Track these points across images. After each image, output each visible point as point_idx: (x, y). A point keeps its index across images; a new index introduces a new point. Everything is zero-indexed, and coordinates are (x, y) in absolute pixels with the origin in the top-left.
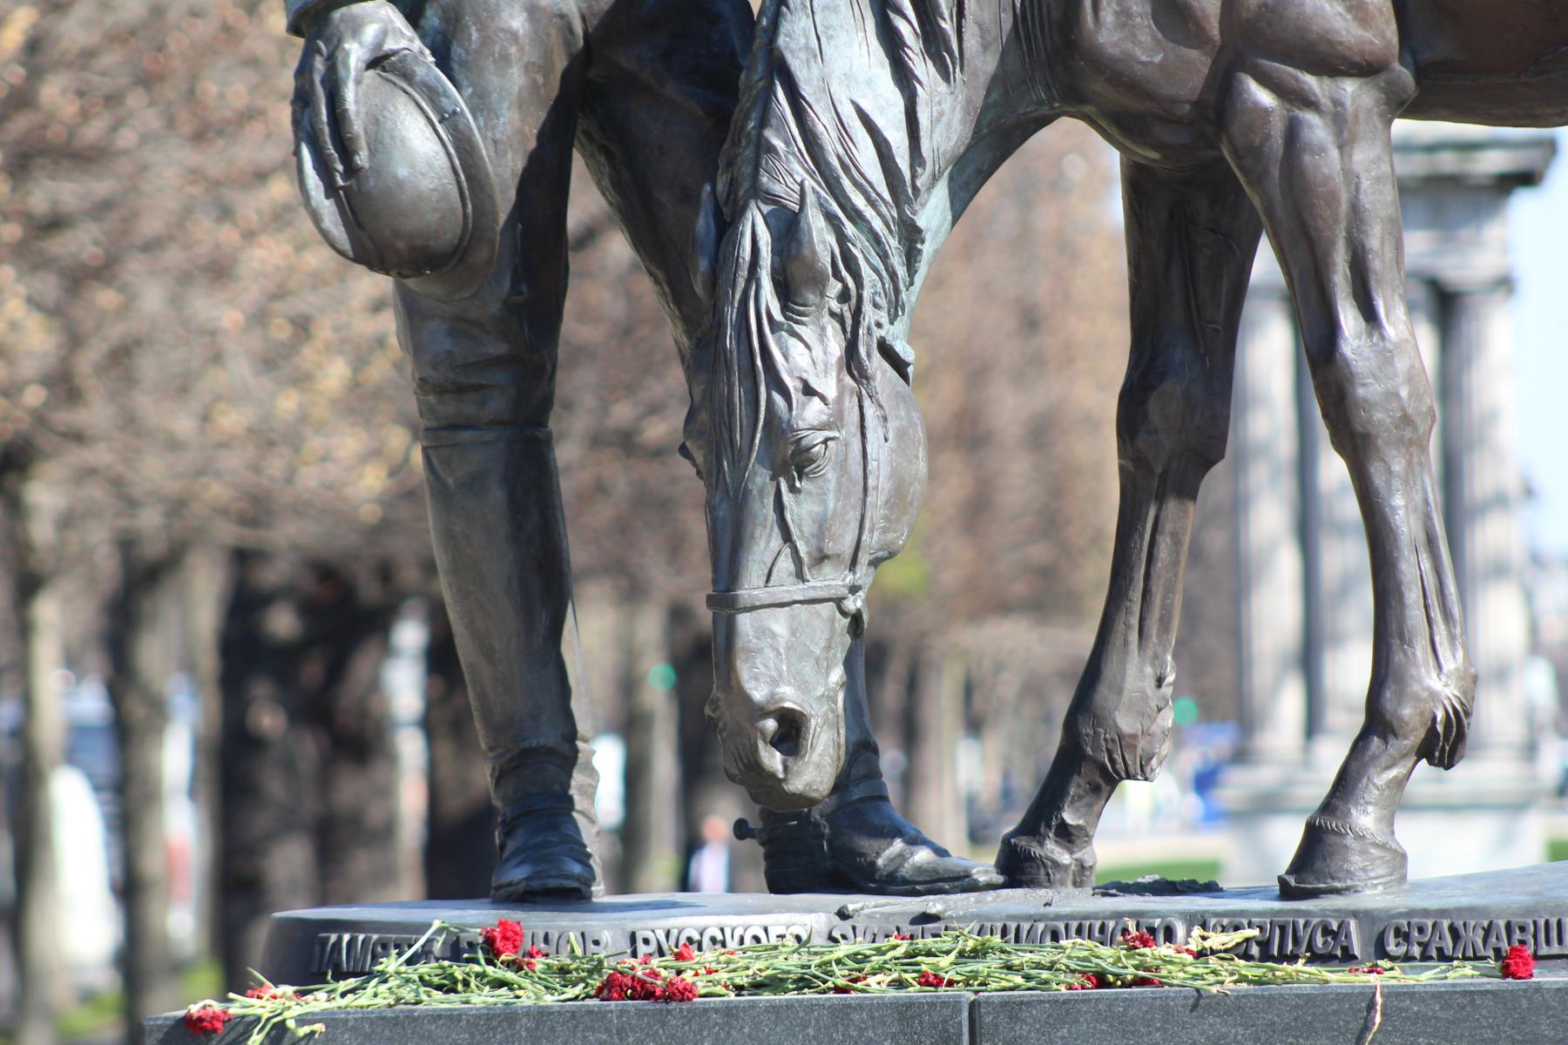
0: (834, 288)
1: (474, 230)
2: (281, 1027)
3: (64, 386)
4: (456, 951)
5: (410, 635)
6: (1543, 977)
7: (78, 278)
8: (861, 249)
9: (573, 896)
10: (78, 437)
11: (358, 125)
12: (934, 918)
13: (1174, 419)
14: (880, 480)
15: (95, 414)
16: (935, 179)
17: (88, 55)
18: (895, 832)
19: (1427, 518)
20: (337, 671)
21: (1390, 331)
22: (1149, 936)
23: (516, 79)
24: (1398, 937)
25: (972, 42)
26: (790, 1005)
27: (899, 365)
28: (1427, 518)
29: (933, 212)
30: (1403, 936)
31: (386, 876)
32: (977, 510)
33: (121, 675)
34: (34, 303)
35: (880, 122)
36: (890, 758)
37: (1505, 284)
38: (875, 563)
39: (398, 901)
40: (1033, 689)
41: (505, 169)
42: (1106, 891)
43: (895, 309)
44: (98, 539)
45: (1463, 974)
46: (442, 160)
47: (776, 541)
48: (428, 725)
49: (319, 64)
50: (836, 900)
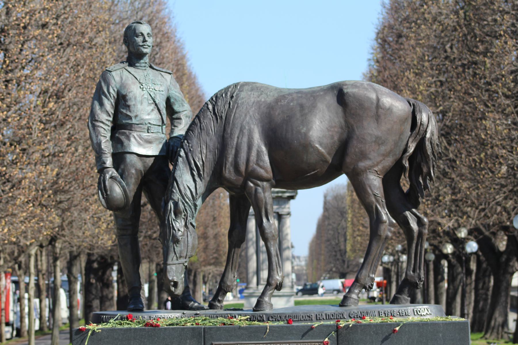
0: (183, 214)
2: (94, 331)
3: (61, 227)
5: (116, 268)
6: (294, 324)
7: (64, 211)
9: (141, 310)
10: (64, 236)
11: (108, 188)
12: (198, 314)
13: (237, 235)
14: (190, 245)
15: (66, 232)
16: (199, 197)
17: (66, 176)
18: (192, 300)
20: (104, 273)
21: (271, 222)
22: (232, 317)
23: (133, 180)
24: (271, 317)
25: (205, 175)
26: (175, 328)
27: (193, 226)
29: (199, 202)
30: (272, 317)
31: (112, 306)
32: (206, 248)
33: (70, 274)
34: (57, 215)
35: (191, 188)
36: (191, 286)
37: (289, 214)
38: (189, 258)
39: (113, 310)
40: (214, 277)
41: (131, 195)
42: (225, 310)
43: (193, 217)
44: (67, 251)
45: (282, 323)
47: (173, 254)
48: (118, 281)
49: (102, 178)
50: (182, 311)
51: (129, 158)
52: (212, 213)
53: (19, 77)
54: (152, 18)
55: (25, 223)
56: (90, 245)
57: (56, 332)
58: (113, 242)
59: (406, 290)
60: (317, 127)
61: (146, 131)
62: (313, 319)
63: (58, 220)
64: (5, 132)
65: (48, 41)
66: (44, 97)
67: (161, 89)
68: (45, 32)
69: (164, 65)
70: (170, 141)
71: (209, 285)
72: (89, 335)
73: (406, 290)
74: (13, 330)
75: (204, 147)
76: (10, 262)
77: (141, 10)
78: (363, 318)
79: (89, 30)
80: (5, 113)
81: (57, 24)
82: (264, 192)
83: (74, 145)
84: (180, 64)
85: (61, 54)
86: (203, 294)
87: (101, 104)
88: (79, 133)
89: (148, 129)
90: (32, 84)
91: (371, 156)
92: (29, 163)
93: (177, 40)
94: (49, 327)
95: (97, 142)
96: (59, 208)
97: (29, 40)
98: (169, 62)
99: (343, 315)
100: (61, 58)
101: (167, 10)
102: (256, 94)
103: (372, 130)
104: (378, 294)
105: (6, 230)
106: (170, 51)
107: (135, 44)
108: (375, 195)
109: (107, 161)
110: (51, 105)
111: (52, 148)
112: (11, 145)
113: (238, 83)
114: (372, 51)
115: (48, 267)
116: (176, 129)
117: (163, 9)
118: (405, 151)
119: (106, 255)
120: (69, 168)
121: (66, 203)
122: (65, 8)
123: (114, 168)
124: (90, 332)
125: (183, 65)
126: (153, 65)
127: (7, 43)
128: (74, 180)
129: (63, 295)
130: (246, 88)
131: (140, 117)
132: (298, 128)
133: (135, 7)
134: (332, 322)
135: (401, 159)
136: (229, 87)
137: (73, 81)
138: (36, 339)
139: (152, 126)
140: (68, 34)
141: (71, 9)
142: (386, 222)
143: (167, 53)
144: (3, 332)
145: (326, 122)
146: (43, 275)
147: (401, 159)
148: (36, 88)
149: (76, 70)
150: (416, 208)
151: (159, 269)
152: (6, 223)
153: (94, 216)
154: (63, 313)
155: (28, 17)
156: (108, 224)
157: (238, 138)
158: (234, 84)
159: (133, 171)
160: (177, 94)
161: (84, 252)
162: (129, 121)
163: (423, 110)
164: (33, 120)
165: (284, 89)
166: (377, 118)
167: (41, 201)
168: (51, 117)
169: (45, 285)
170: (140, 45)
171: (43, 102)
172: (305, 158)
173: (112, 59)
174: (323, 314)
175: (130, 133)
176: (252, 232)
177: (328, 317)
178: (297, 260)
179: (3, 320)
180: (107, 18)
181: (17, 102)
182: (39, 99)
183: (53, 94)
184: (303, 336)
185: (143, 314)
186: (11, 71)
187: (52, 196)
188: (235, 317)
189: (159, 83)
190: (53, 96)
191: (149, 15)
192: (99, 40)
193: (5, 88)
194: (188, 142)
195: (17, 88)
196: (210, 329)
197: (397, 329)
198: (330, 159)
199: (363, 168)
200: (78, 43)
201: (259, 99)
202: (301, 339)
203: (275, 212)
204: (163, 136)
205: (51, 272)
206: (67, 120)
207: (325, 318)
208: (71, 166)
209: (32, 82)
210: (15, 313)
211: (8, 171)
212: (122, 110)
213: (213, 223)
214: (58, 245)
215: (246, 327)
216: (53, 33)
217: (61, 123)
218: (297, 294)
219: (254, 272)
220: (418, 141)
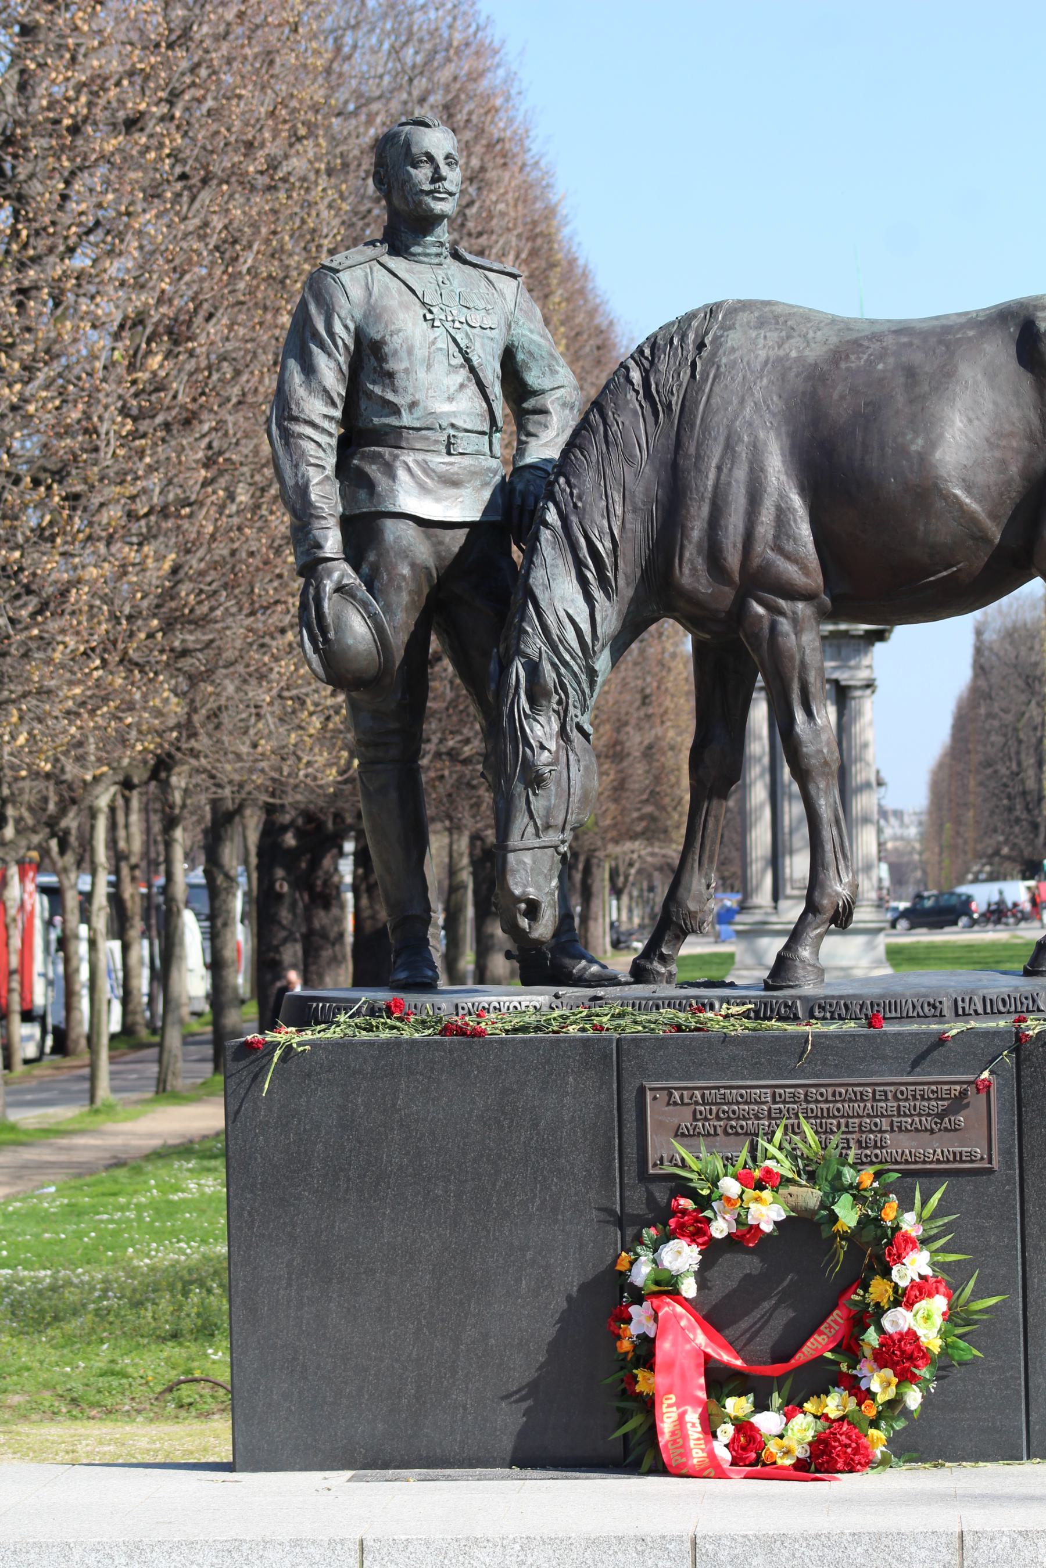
1: (385, 668)
3: (187, 728)
4: (373, 1012)
5: (349, 846)
6: (888, 1028)
9: (428, 986)
10: (194, 753)
11: (329, 620)
14: (577, 790)
15: (202, 743)
16: (603, 647)
17: (202, 573)
18: (582, 957)
19: (836, 810)
20: (315, 864)
21: (819, 721)
22: (702, 1008)
23: (405, 598)
25: (621, 582)
26: (531, 1039)
27: (586, 735)
28: (836, 810)
29: (602, 662)
30: (822, 1008)
32: (620, 788)
33: (213, 864)
34: (174, 691)
35: (578, 620)
41: (398, 640)
42: (682, 985)
44: (203, 798)
45: (850, 1026)
47: (526, 819)
48: (355, 888)
49: (312, 590)
51: (395, 532)
52: (639, 682)
53: (60, 280)
54: (457, 97)
55: (78, 715)
56: (273, 780)
57: (174, 1038)
58: (341, 773)
60: (957, 434)
61: (444, 451)
62: (945, 1012)
63: (176, 708)
64: (16, 445)
65: (145, 171)
66: (131, 340)
67: (487, 323)
68: (136, 143)
69: (494, 237)
70: (516, 480)
71: (631, 898)
72: (275, 1060)
74: (44, 1033)
75: (618, 498)
76: (34, 831)
77: (422, 73)
79: (267, 135)
80: (18, 387)
81: (172, 118)
82: (798, 633)
83: (223, 482)
84: (541, 234)
85: (185, 208)
86: (612, 925)
87: (309, 369)
88: (237, 444)
89: (449, 444)
90: (98, 299)
92: (89, 538)
93: (531, 162)
94: (151, 1026)
95: (297, 483)
96: (179, 670)
97: (88, 167)
98: (509, 230)
99: (1034, 1001)
100: (185, 218)
101: (501, 72)
102: (773, 336)
105: (22, 739)
106: (510, 197)
109: (326, 539)
110: (154, 362)
111: (157, 490)
112: (36, 482)
113: (719, 305)
115: (147, 844)
116: (533, 443)
117: (488, 69)
119: (321, 809)
120: (210, 550)
121: (200, 655)
122: (194, 69)
123: (346, 560)
124: (278, 1053)
125: (549, 238)
126: (462, 251)
127: (22, 177)
128: (225, 586)
129: (191, 930)
130: (743, 317)
131: (425, 408)
132: (900, 440)
133: (403, 65)
134: (1002, 1023)
136: (691, 317)
137: (221, 289)
138: (112, 1060)
139: (460, 434)
140: (204, 148)
141: (214, 73)
143: (500, 199)
144: (16, 1039)
145: (986, 421)
146: (133, 868)
148: (109, 309)
149: (227, 256)
151: (478, 851)
152: (21, 718)
153: (286, 694)
154: (194, 981)
155: (83, 99)
156: (328, 718)
157: (719, 468)
158: (706, 306)
159: (406, 571)
160: (536, 337)
161: (255, 800)
162: (393, 421)
164: (100, 409)
165: (856, 320)
167: (125, 652)
168: (153, 398)
169: (138, 899)
170: (422, 191)
171: (131, 352)
172: (922, 528)
173: (336, 222)
174: (975, 998)
175: (396, 457)
176: (760, 738)
177: (991, 1008)
178: (893, 820)
179: (16, 1006)
180: (319, 97)
181: (51, 355)
182: (119, 345)
183: (161, 329)
184: (915, 1064)
185: (437, 999)
186: (35, 260)
187: (160, 635)
188: (712, 1007)
189: (481, 305)
190: (160, 336)
191: (447, 88)
192: (297, 165)
193: (18, 314)
194: (568, 482)
195: (52, 314)
196: (636, 1042)
200: (233, 173)
201: (781, 353)
202: (909, 1074)
203: (829, 681)
204: (494, 463)
205: (158, 859)
206: (201, 406)
207: (980, 1010)
208: (214, 546)
209: (98, 292)
210: (50, 983)
211: (26, 562)
212: (371, 387)
213: (642, 713)
214: (178, 780)
215: (745, 1037)
216: (161, 145)
217: (185, 415)
218: (893, 925)
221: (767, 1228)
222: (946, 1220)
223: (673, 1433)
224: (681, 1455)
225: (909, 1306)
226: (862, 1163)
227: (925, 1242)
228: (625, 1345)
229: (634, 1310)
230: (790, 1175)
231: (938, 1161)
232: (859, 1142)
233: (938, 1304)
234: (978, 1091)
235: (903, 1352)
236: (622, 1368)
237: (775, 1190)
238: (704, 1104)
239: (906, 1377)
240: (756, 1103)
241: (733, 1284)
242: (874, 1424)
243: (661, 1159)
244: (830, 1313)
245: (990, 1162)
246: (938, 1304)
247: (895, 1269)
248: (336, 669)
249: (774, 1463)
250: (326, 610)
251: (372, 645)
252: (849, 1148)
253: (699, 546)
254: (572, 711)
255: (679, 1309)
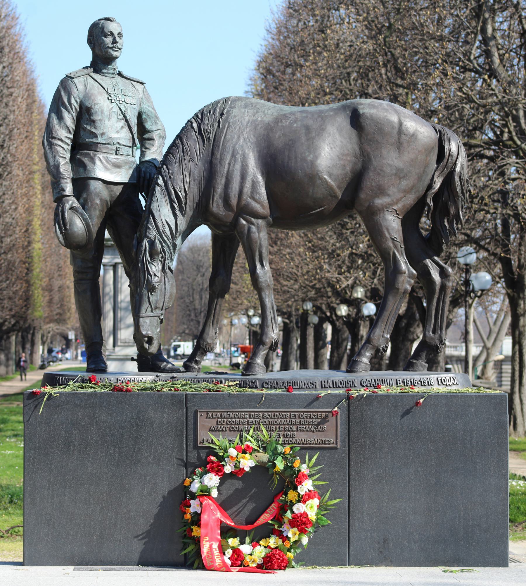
1: (88, 242)
4: (83, 381)
6: (295, 392)
8: (166, 248)
11: (67, 221)
14: (168, 293)
19: (272, 303)
23: (97, 213)
25: (188, 209)
28: (272, 303)
29: (178, 241)
32: (50, 301)
35: (170, 224)
41: (95, 230)
42: (207, 373)
45: (279, 391)
46: (83, 228)
47: (148, 304)
49: (60, 208)
51: (95, 186)
59: (424, 354)
70: (141, 167)
73: (424, 354)
78: (378, 387)
87: (60, 118)
89: (117, 151)
91: (390, 192)
102: (251, 111)
103: (393, 161)
104: (243, 360)
107: (102, 45)
108: (393, 239)
114: (250, 82)
118: (430, 187)
124: (46, 397)
130: (239, 103)
134: (341, 391)
135: (425, 196)
142: (405, 273)
145: (338, 149)
147: (425, 196)
150: (438, 256)
157: (229, 164)
158: (223, 98)
159: (98, 202)
163: (451, 138)
166: (399, 146)
175: (95, 155)
176: (109, 285)
177: (335, 385)
189: (130, 94)
194: (167, 168)
197: (421, 401)
198: (339, 194)
199: (380, 206)
201: (254, 118)
207: (331, 386)
219: (110, 332)
220: (445, 176)
221: (247, 469)
222: (319, 467)
223: (208, 553)
224: (211, 562)
225: (304, 502)
226: (285, 444)
227: (311, 476)
228: (188, 516)
229: (192, 502)
230: (256, 448)
231: (316, 444)
232: (284, 435)
233: (315, 502)
234: (333, 415)
235: (302, 521)
236: (185, 526)
237: (251, 454)
238: (221, 418)
239: (302, 531)
240: (243, 418)
241: (231, 492)
242: (289, 550)
243: (203, 440)
244: (271, 505)
245: (337, 444)
246: (315, 502)
247: (299, 487)
248: (69, 240)
249: (248, 566)
250: (66, 216)
251: (84, 231)
252: (280, 437)
253: (220, 195)
254: (167, 261)
255: (210, 502)
